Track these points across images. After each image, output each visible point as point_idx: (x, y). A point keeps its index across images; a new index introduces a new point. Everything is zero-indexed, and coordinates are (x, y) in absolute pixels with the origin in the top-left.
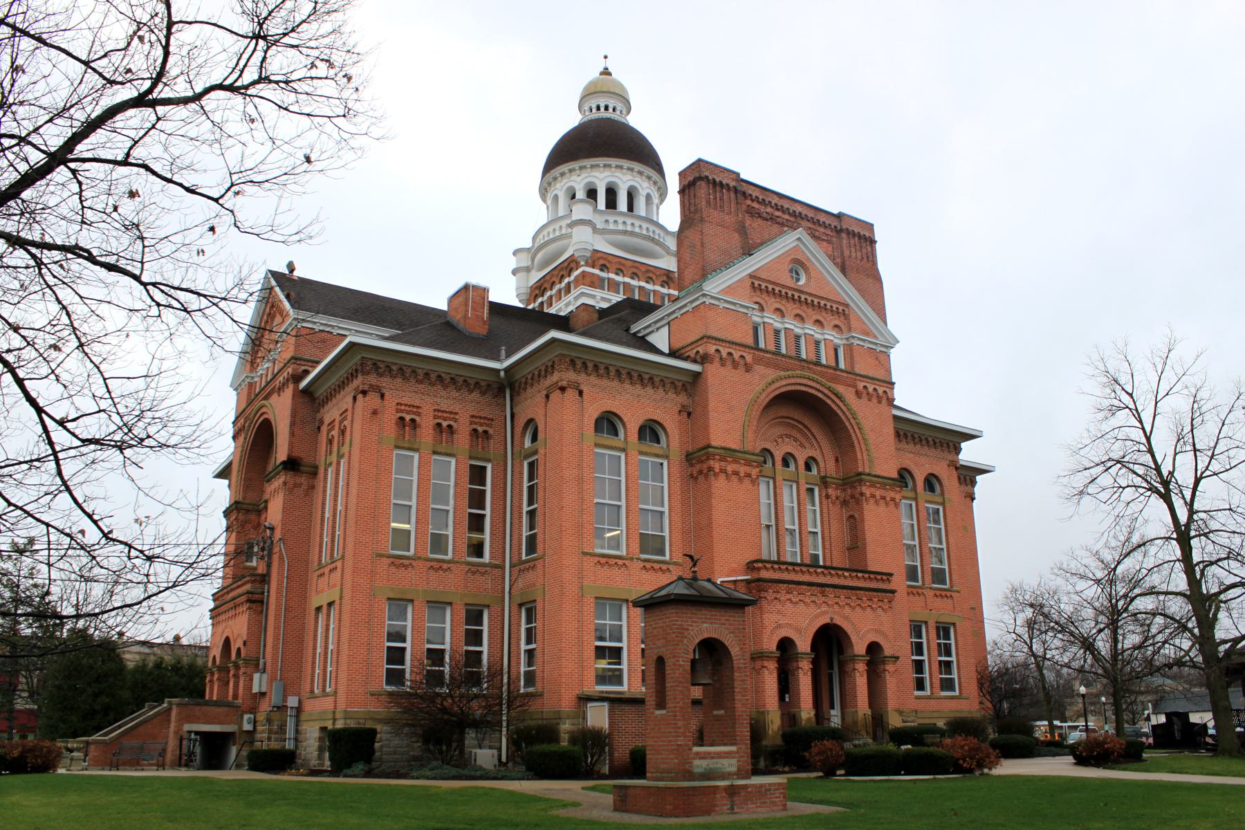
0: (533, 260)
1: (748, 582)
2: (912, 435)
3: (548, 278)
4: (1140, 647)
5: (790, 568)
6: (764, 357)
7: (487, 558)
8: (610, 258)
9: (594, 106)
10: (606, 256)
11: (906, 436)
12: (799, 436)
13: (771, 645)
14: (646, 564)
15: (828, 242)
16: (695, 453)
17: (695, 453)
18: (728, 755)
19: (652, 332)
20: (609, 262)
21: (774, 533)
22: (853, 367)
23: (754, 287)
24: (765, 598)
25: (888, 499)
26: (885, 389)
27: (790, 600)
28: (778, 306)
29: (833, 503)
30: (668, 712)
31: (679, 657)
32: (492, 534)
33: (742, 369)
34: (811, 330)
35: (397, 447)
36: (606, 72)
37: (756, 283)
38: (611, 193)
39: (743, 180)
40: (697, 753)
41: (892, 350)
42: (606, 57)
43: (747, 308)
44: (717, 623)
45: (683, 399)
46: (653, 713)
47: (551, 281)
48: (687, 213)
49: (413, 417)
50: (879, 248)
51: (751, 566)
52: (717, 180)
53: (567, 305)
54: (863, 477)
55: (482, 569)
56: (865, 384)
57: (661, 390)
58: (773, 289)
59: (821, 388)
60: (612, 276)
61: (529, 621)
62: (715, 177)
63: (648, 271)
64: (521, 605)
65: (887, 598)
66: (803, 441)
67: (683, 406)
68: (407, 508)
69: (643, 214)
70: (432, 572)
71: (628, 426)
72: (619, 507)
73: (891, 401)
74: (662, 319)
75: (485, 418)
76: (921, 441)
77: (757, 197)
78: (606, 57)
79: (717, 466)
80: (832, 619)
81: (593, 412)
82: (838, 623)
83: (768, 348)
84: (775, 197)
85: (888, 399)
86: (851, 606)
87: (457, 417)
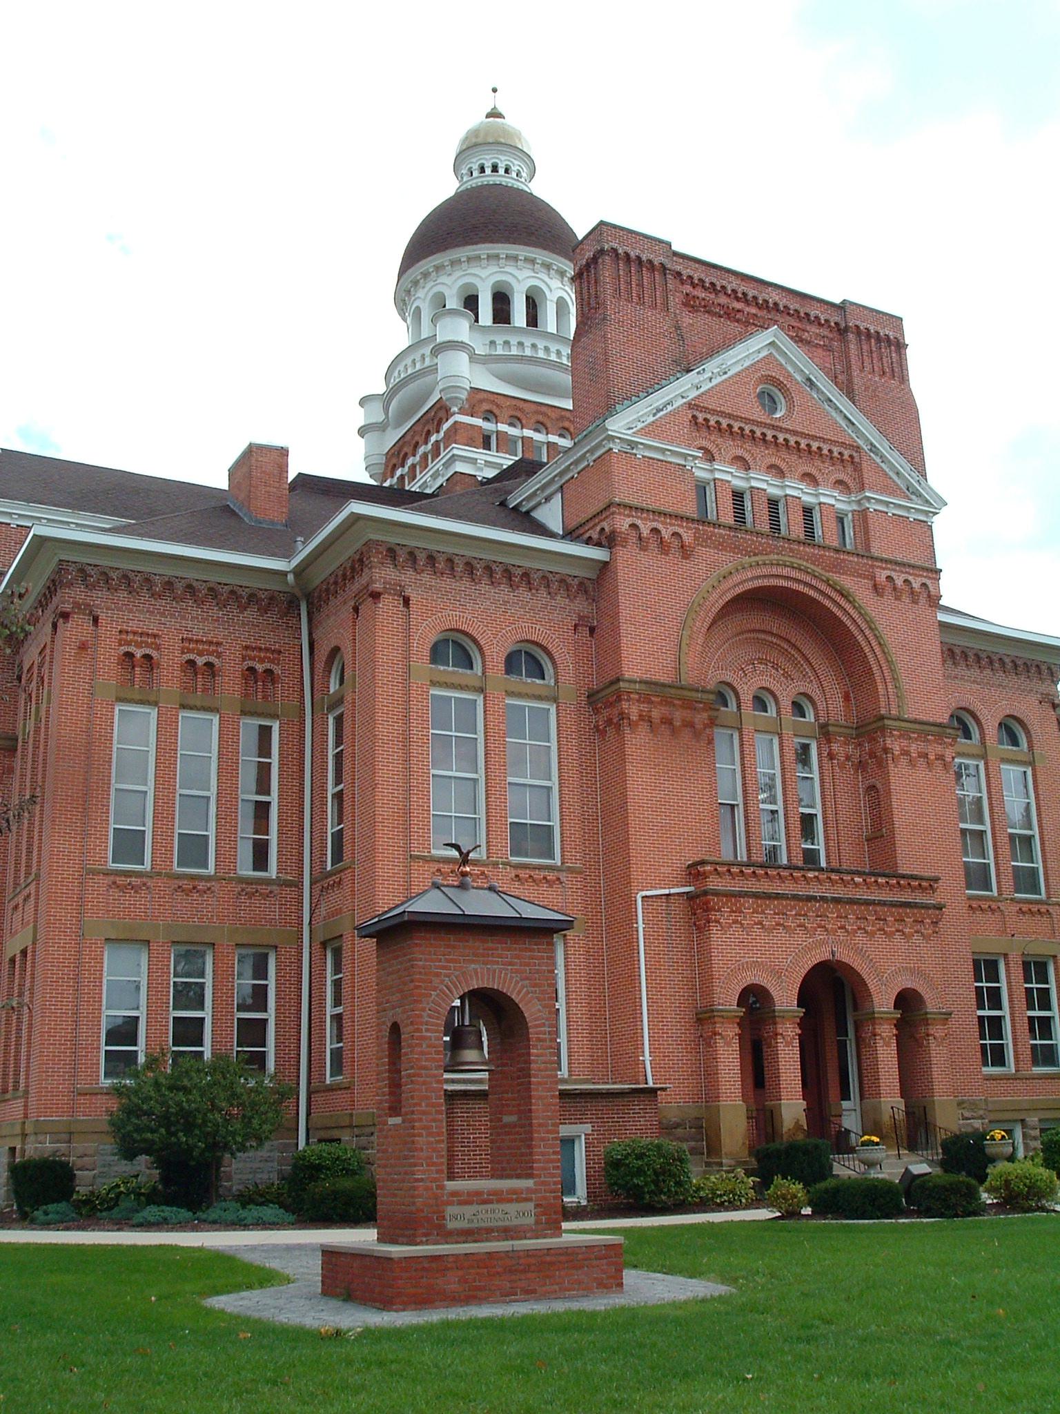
0: (387, 413)
1: (690, 897)
2: (976, 655)
3: (408, 438)
4: (189, 992)
5: (760, 872)
6: (713, 534)
7: (273, 871)
8: (500, 400)
9: (475, 167)
10: (491, 397)
11: (965, 656)
12: (781, 661)
13: (727, 999)
14: (519, 871)
15: (828, 349)
16: (602, 690)
17: (602, 690)
18: (516, 1196)
19: (539, 504)
20: (498, 406)
21: (742, 818)
22: (868, 547)
23: (696, 423)
24: (717, 921)
25: (932, 757)
26: (924, 580)
27: (760, 923)
28: (740, 452)
29: (842, 766)
30: (404, 1121)
31: (422, 1024)
32: (280, 833)
33: (675, 553)
34: (797, 490)
35: (120, 700)
36: (494, 114)
37: (701, 417)
38: (502, 302)
39: (675, 254)
40: (454, 1194)
41: (935, 519)
42: (495, 90)
43: (685, 456)
44: (497, 963)
45: (580, 605)
46: (386, 1123)
47: (414, 442)
48: (586, 309)
49: (148, 651)
50: (910, 353)
51: (694, 872)
52: (632, 254)
53: (435, 476)
54: (887, 722)
55: (263, 889)
56: (888, 573)
57: (543, 592)
58: (729, 426)
59: (814, 582)
60: (503, 427)
61: (337, 968)
62: (628, 249)
63: (562, 418)
64: (324, 945)
65: (929, 916)
66: (789, 668)
67: (581, 618)
68: (142, 795)
69: (552, 328)
70: (179, 896)
71: (487, 653)
72: (549, 789)
73: (934, 600)
74: (552, 481)
75: (267, 650)
76: (991, 662)
77: (700, 280)
78: (495, 90)
79: (633, 710)
80: (833, 953)
81: (427, 633)
82: (846, 960)
83: (722, 520)
84: (732, 278)
85: (929, 596)
86: (866, 932)
87: (220, 650)
